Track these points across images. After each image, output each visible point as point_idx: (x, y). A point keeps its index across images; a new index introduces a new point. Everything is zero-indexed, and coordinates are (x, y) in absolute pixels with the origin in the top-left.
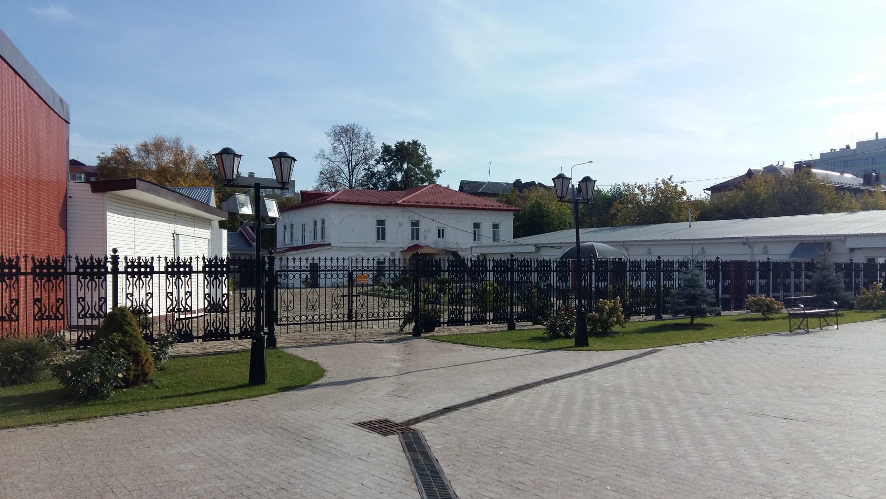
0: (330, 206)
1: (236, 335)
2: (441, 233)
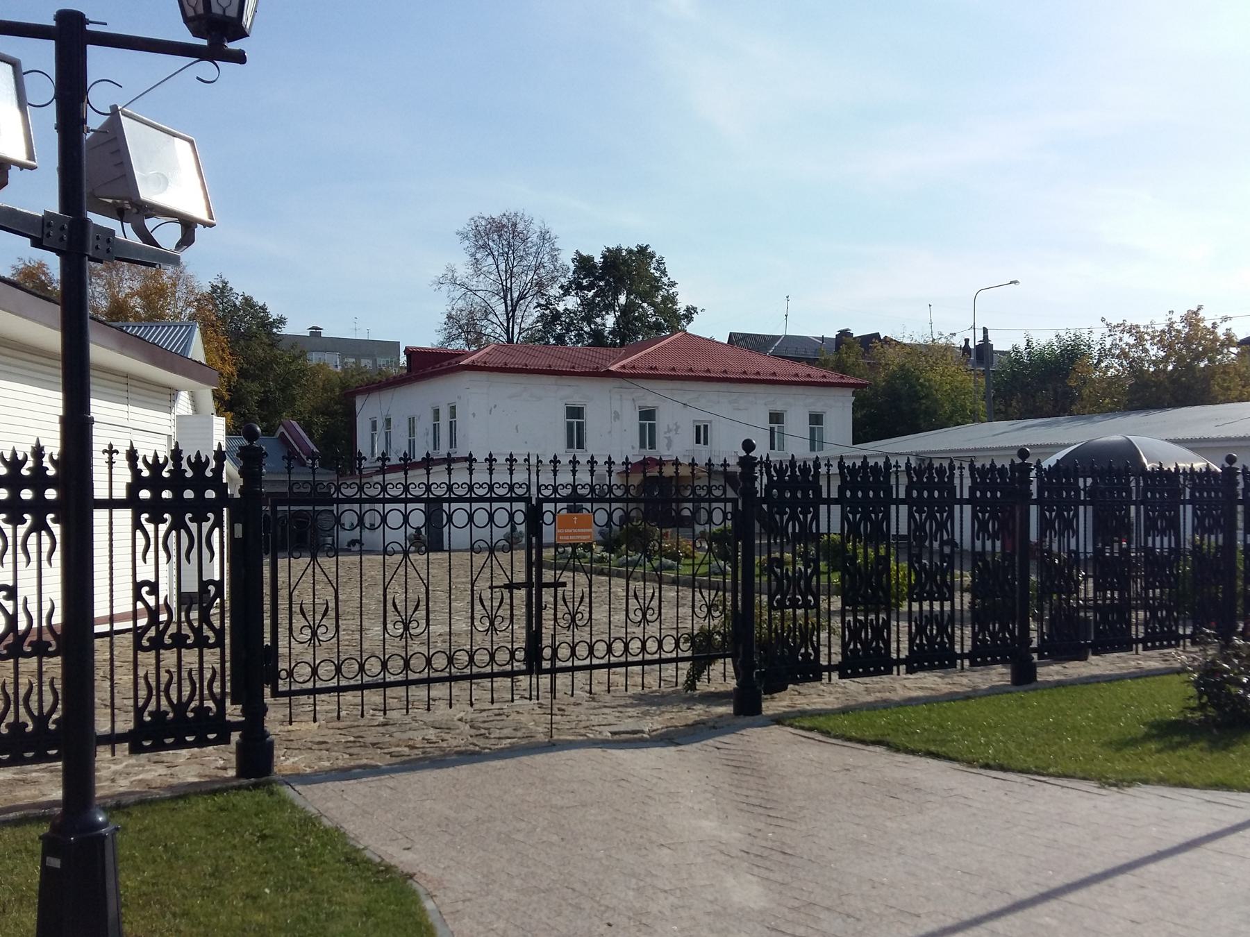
0: (466, 378)
1: (121, 738)
2: (701, 434)
